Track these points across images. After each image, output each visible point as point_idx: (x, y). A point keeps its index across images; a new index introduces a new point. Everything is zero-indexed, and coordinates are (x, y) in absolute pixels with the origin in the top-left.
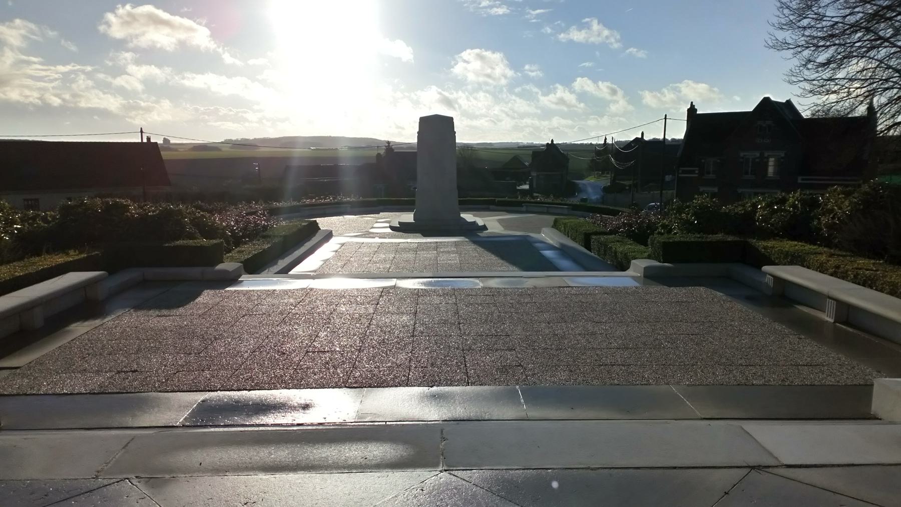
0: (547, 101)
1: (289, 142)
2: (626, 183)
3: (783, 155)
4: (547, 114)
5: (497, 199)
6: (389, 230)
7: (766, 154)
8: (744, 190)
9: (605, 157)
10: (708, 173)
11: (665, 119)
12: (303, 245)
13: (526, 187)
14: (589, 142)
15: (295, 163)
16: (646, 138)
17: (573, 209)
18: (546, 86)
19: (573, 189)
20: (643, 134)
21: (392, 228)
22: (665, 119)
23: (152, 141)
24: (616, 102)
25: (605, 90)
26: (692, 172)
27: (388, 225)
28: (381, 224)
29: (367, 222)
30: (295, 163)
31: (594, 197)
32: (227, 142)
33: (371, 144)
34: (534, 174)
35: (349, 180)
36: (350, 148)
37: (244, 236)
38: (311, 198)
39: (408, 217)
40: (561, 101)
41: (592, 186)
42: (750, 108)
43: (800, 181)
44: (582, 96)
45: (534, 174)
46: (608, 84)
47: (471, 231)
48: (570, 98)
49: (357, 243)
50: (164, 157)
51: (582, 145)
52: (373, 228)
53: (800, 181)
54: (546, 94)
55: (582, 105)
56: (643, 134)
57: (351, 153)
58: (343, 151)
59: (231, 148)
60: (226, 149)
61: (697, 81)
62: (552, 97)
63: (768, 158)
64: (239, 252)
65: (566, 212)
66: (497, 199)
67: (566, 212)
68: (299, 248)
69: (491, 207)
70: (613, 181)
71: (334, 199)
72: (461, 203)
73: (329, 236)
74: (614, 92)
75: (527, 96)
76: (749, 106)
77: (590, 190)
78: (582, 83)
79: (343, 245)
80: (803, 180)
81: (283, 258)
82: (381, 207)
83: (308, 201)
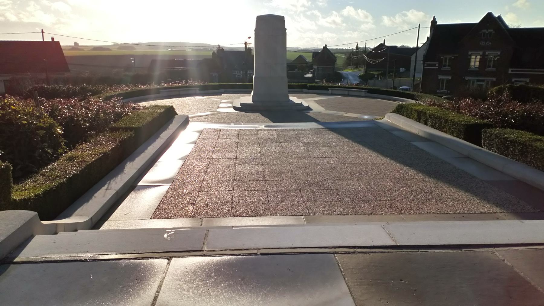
0: (323, 22)
1: (156, 46)
2: (376, 73)
3: (499, 54)
4: (321, 29)
5: (308, 85)
6: (232, 110)
7: (487, 53)
8: (470, 78)
9: (356, 57)
10: (445, 66)
11: (419, 27)
12: (158, 137)
13: (310, 75)
14: (341, 48)
15: (159, 58)
16: (387, 44)
17: (368, 92)
18: (326, 12)
19: (339, 77)
20: (384, 41)
21: (235, 108)
22: (419, 27)
23: (55, 40)
24: (367, 23)
25: (361, 14)
26: (435, 65)
27: (230, 105)
28: (226, 103)
29: (213, 102)
30: (159, 58)
31: (355, 83)
32: (116, 45)
33: (206, 47)
34: (315, 67)
35: (193, 70)
36: (193, 50)
37: (90, 129)
38: (169, 83)
39: (248, 99)
40: (334, 22)
41: (353, 75)
42: (478, 21)
43: (510, 72)
44: (347, 19)
45: (315, 67)
46: (365, 12)
47: (301, 114)
48: (338, 20)
49: (215, 130)
50: (65, 55)
51: (337, 49)
52: (219, 108)
53: (510, 72)
54: (323, 18)
55: (344, 25)
56: (384, 41)
57: (194, 53)
58: (189, 51)
59: (118, 49)
60: (114, 49)
61: (418, 10)
62: (329, 19)
63: (470, 55)
64: (71, 159)
65: (363, 94)
66: (308, 85)
67: (363, 94)
68: (154, 140)
69: (304, 90)
70: (366, 72)
71: (186, 83)
72: (290, 87)
73: (186, 121)
74: (366, 17)
75: (313, 18)
76: (477, 19)
77: (351, 77)
78: (349, 11)
79: (201, 132)
80: (512, 71)
81: (133, 160)
82: (223, 90)
83: (166, 85)
